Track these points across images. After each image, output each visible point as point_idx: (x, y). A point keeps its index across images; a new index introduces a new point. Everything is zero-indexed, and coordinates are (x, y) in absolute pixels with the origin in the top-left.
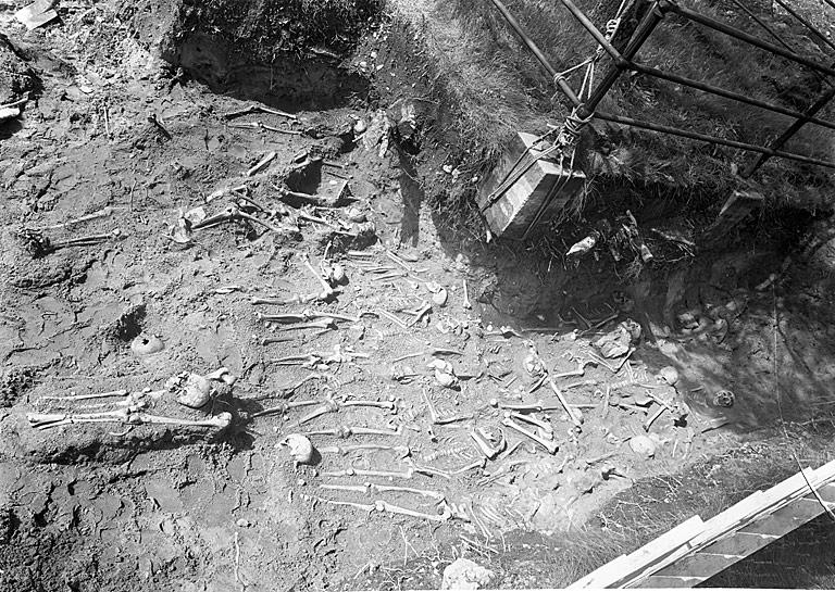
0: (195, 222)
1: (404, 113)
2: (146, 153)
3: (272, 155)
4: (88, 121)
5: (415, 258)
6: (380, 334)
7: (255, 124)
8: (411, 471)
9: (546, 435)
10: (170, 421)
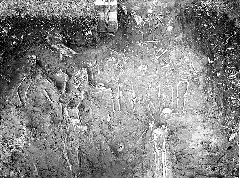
0: (79, 122)
1: (58, 38)
2: (38, 134)
3: (44, 90)
4: (15, 153)
5: (96, 61)
6: (126, 80)
7: (26, 93)
8: (172, 86)
9: (163, 50)
10: (164, 141)
